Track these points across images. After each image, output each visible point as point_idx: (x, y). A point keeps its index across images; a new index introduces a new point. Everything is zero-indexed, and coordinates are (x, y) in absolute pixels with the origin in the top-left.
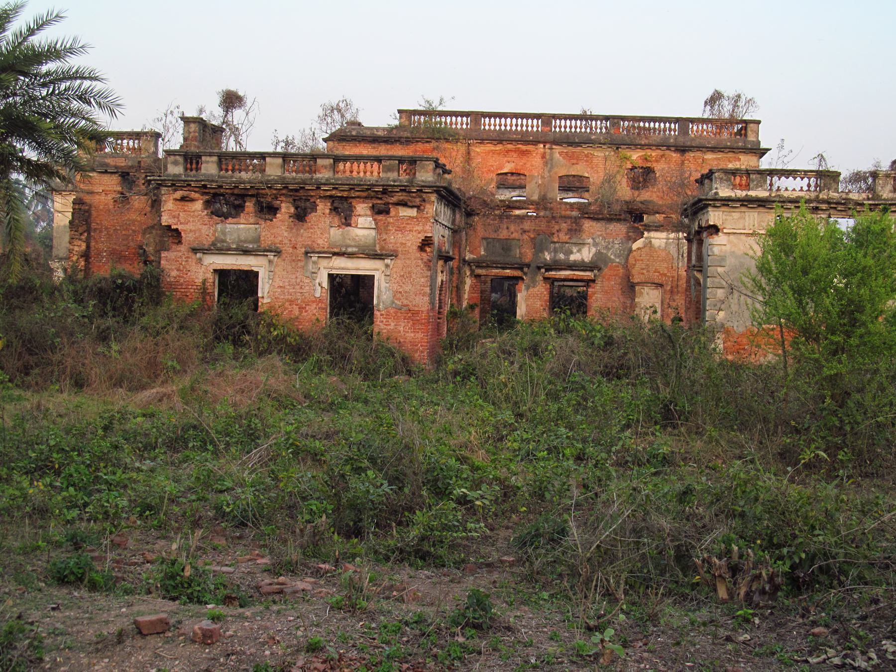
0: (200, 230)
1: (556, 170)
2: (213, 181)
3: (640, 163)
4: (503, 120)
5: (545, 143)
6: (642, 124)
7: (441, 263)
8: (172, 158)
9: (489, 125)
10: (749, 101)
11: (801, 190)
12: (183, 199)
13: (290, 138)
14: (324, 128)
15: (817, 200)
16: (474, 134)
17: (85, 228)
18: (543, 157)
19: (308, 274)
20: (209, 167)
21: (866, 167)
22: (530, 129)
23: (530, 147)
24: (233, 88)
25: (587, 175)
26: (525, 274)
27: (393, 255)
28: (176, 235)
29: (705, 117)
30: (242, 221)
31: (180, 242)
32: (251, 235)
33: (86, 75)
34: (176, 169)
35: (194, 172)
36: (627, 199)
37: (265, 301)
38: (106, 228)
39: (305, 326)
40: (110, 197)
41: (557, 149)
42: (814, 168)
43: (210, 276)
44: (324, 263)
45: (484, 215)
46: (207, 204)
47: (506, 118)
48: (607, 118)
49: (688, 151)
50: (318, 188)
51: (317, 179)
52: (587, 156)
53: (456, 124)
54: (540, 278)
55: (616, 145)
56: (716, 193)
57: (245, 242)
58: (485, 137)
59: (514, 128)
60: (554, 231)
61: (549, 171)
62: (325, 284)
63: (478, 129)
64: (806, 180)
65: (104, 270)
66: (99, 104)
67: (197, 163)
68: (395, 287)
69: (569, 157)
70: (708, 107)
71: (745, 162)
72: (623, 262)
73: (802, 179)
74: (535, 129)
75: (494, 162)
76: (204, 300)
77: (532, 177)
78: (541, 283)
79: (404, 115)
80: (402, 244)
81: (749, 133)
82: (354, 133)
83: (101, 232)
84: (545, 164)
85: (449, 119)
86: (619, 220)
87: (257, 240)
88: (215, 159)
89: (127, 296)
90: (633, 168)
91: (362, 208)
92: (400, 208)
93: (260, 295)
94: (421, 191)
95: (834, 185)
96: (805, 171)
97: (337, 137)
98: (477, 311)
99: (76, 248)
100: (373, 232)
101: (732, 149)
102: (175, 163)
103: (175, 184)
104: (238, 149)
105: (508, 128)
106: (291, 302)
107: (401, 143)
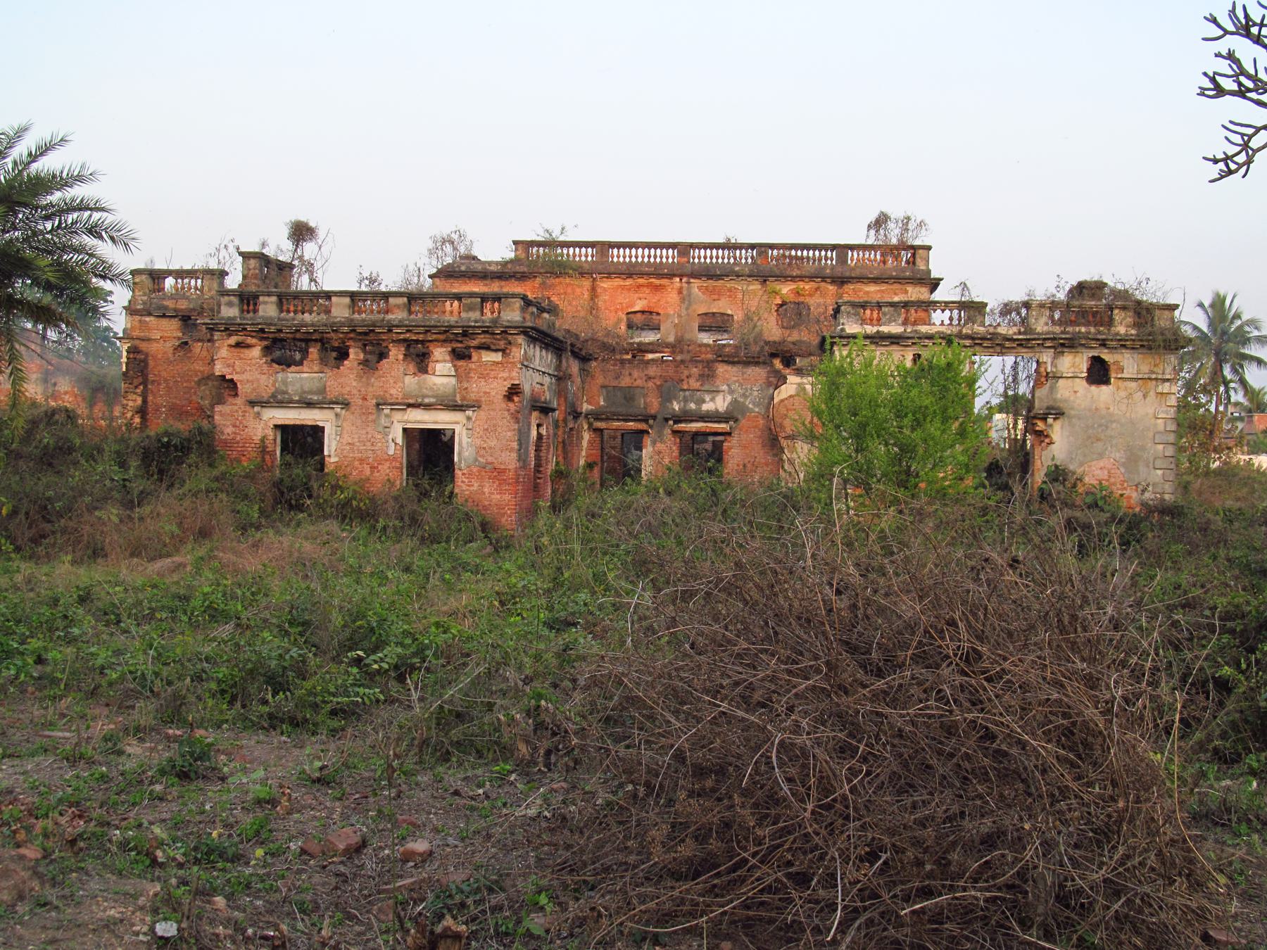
0: (258, 380)
1: (694, 307)
2: (271, 324)
3: (792, 298)
4: (634, 251)
5: (681, 276)
6: (793, 253)
7: (535, 414)
8: (226, 298)
9: (617, 256)
10: (921, 224)
11: (942, 324)
12: (238, 345)
13: (374, 275)
14: (434, 263)
15: (960, 336)
16: (600, 267)
17: (140, 380)
18: (680, 291)
19: (381, 429)
20: (268, 309)
21: (1018, 296)
22: (664, 260)
23: (664, 281)
24: (303, 219)
25: (729, 312)
26: (651, 427)
27: (476, 406)
28: (230, 386)
29: (869, 242)
30: (305, 369)
31: (236, 395)
32: (316, 385)
33: (92, 205)
34: (230, 311)
35: (251, 314)
36: (777, 339)
37: (333, 460)
38: (166, 380)
39: (375, 489)
40: (169, 344)
41: (696, 283)
42: (957, 299)
43: (270, 433)
44: (397, 416)
45: (603, 360)
46: (267, 350)
47: (637, 248)
48: (753, 246)
49: (847, 282)
50: (390, 331)
51: (389, 321)
52: (730, 290)
53: (580, 256)
54: (667, 431)
55: (763, 276)
56: (843, 330)
57: (311, 392)
58: (612, 270)
59: (646, 260)
60: (684, 377)
61: (687, 309)
62: (400, 440)
63: (603, 263)
64: (947, 313)
65: (161, 424)
66: (112, 238)
67: (255, 304)
68: (478, 442)
69: (706, 290)
70: (872, 232)
71: (915, 293)
72: (763, 412)
73: (943, 311)
74: (658, 260)
75: (623, 299)
76: (264, 460)
77: (668, 316)
78: (670, 436)
79: (520, 247)
80: (485, 393)
81: (918, 261)
82: (463, 268)
83: (159, 384)
84: (683, 300)
85: (571, 250)
86: (757, 364)
87: (322, 391)
88: (274, 299)
89: (171, 456)
90: (784, 304)
91: (440, 353)
92: (483, 352)
93: (326, 453)
94: (505, 332)
95: (979, 319)
96: (946, 303)
97: (446, 273)
98: (596, 470)
99: (131, 403)
100: (453, 380)
101: (899, 280)
102: (230, 304)
103: (229, 328)
104: (314, 289)
105: (640, 260)
106: (361, 461)
107: (518, 279)
